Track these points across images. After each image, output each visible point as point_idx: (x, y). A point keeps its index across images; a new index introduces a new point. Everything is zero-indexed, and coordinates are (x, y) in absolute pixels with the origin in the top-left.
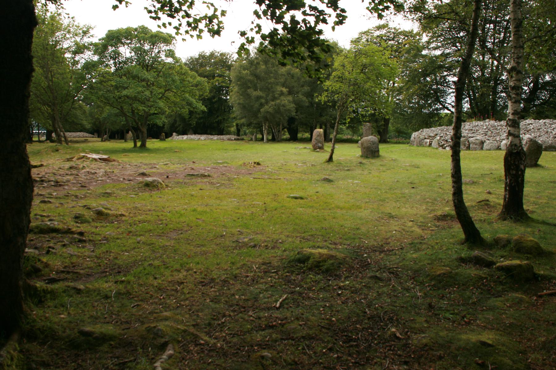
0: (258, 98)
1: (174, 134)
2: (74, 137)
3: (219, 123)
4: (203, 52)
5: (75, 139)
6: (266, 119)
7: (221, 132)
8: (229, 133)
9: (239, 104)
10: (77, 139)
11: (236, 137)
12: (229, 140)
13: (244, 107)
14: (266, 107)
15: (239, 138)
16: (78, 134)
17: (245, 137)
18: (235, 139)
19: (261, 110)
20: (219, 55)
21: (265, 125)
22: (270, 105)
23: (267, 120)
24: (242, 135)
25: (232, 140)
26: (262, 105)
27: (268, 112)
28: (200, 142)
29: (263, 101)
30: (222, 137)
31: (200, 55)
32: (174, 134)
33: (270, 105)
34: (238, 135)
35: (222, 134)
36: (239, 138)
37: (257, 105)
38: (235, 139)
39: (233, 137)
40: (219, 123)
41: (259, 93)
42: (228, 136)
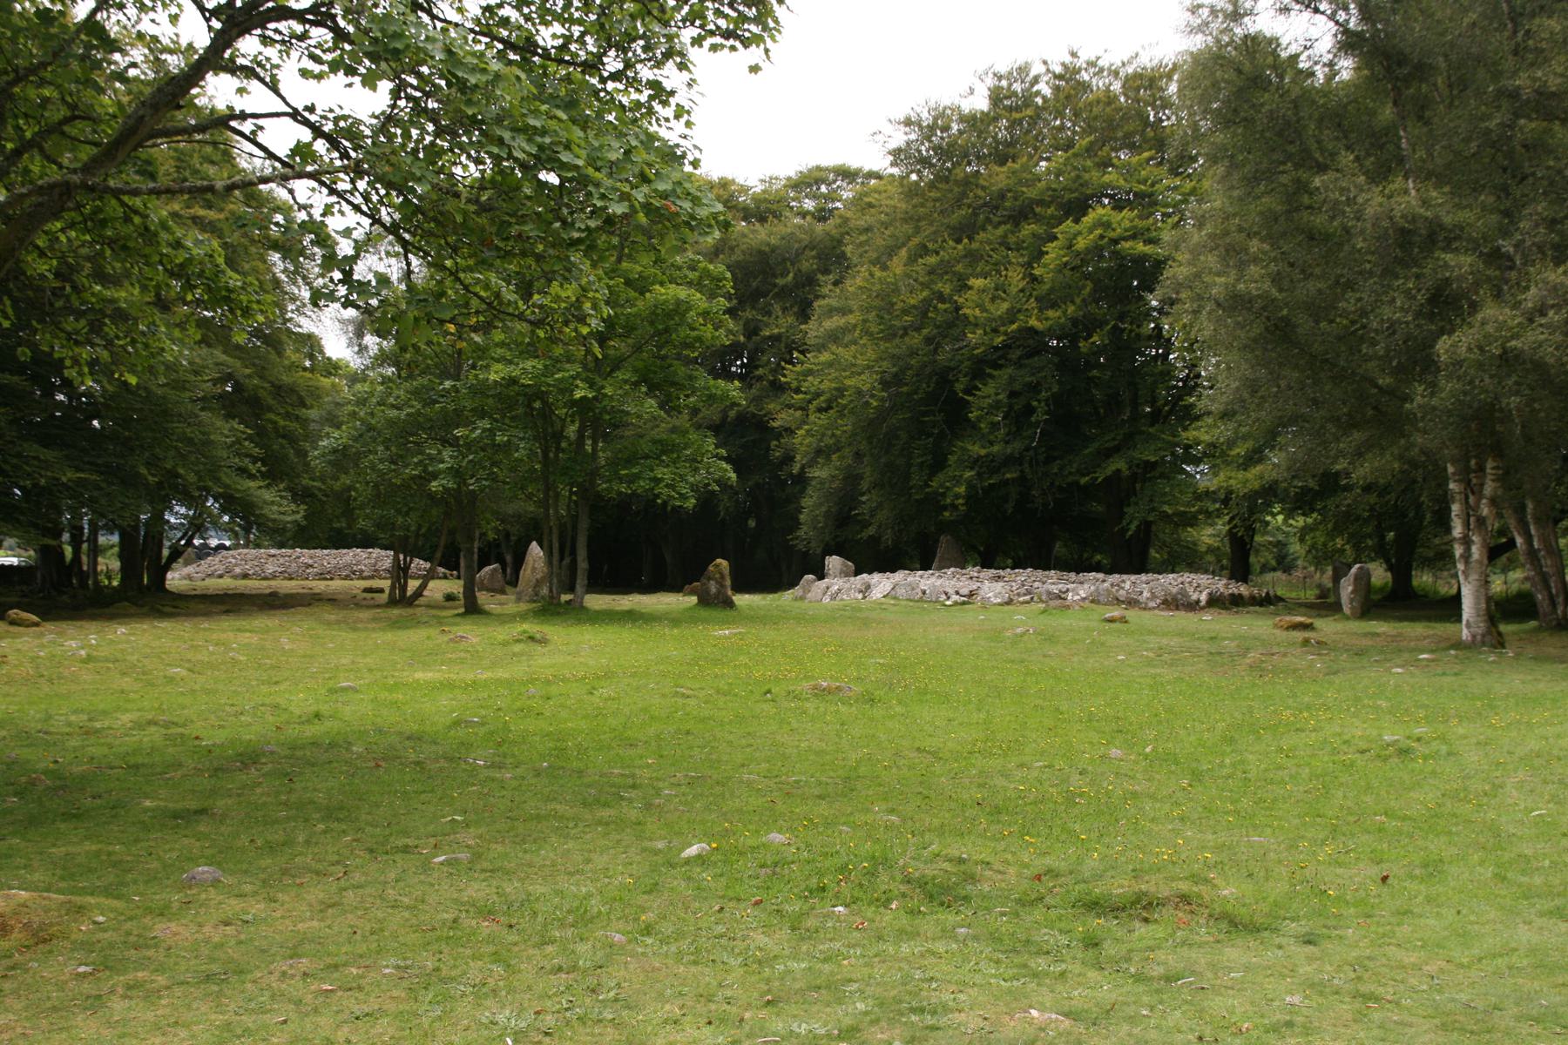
0: (1411, 242)
1: (834, 562)
2: (321, 576)
3: (1120, 491)
4: (1023, 70)
5: (320, 586)
6: (1482, 432)
7: (1132, 557)
8: (1184, 559)
9: (1236, 303)
10: (337, 584)
11: (1221, 585)
12: (1175, 603)
13: (1275, 333)
14: (1492, 313)
15: (1243, 589)
16: (349, 556)
17: (1276, 583)
18: (1215, 602)
19: (1443, 345)
20: (1117, 87)
21: (1477, 490)
22: (1532, 296)
23: (1498, 450)
24: (1265, 568)
25: (1193, 606)
26: (1446, 305)
27: (1508, 360)
28: (971, 616)
29: (1460, 264)
30: (1128, 583)
31: (996, 97)
32: (834, 562)
33: (1532, 296)
34: (1240, 571)
35: (1132, 560)
36: (1243, 589)
37: (1396, 308)
38: (1215, 602)
39: (1200, 585)
40: (1120, 491)
41: (1408, 198)
42: (1169, 582)
